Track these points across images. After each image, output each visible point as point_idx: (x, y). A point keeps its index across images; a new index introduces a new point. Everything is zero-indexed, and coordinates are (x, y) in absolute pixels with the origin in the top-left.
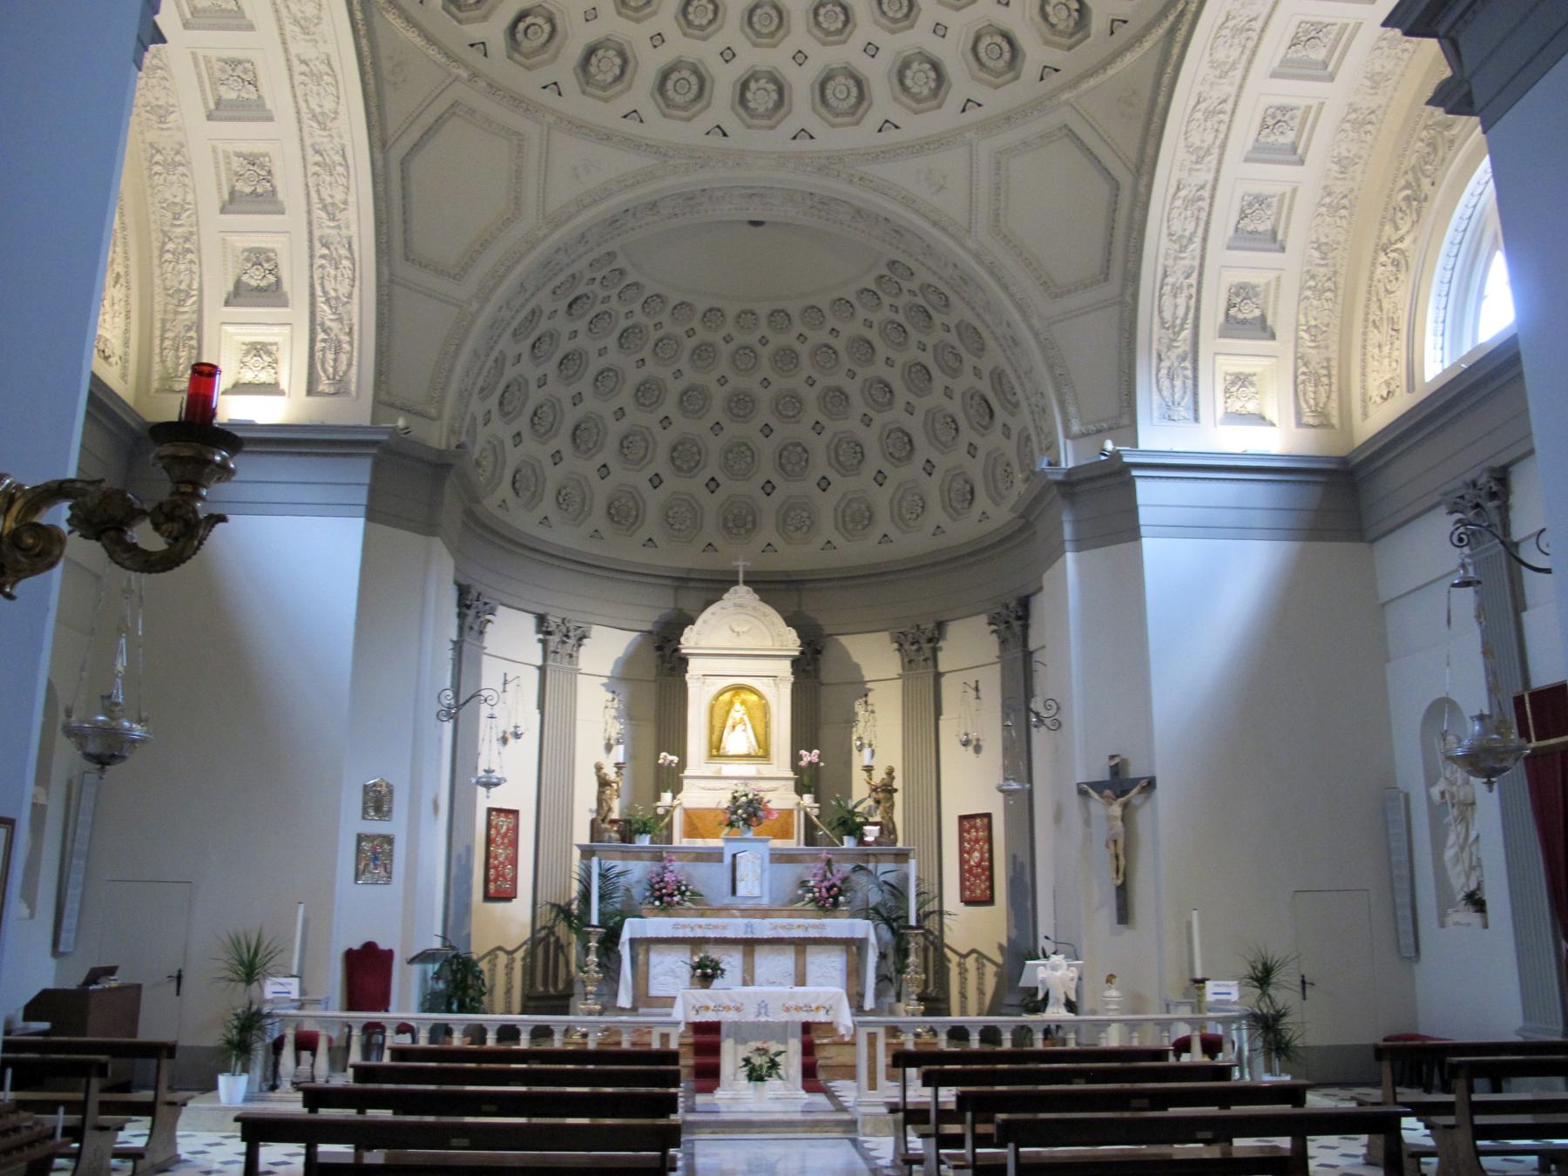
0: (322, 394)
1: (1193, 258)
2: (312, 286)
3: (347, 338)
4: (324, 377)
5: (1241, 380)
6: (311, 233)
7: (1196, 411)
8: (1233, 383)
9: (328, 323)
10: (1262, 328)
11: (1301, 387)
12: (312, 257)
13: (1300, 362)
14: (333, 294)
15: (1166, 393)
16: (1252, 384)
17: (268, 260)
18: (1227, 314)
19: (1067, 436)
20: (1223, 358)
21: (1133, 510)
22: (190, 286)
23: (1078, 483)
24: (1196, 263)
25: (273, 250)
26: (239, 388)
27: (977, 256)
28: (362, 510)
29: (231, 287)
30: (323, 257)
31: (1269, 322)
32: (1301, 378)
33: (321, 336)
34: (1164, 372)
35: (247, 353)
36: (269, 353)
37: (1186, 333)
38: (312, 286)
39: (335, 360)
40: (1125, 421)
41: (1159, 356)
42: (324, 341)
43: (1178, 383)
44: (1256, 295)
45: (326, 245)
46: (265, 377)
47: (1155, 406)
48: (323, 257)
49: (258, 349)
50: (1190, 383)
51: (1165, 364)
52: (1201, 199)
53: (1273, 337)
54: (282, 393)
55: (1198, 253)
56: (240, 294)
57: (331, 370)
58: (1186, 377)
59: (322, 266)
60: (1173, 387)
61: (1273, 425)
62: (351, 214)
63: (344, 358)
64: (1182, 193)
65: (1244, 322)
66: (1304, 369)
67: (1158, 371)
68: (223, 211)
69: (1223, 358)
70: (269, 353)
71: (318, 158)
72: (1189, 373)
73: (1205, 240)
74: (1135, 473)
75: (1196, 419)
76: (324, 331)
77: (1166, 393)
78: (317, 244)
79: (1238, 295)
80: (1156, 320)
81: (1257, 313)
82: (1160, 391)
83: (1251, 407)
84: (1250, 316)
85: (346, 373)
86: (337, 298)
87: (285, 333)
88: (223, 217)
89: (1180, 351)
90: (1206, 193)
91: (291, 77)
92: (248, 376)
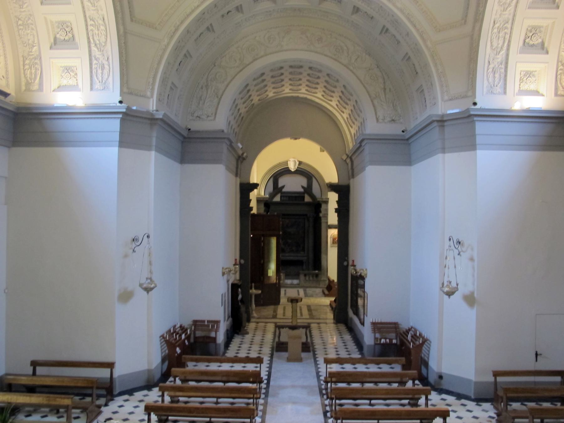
0: (97, 90)
1: (510, 14)
2: (88, 38)
3: (107, 63)
4: (98, 82)
5: (529, 74)
6: (85, 16)
7: (505, 88)
8: (525, 75)
9: (97, 56)
10: (542, 48)
11: (559, 76)
12: (87, 25)
13: (560, 64)
14: (98, 42)
15: (491, 80)
16: (534, 75)
17: (67, 27)
18: (524, 41)
19: (442, 100)
20: (520, 64)
21: (474, 135)
22: (34, 42)
23: (446, 121)
24: (511, 17)
25: (69, 22)
26: (61, 88)
27: (401, 11)
28: (118, 143)
29: (52, 40)
30: (91, 25)
31: (546, 45)
32: (559, 72)
33: (94, 62)
34: (490, 70)
35: (63, 71)
36: (73, 71)
37: (503, 52)
38: (88, 38)
39: (102, 73)
40: (470, 94)
41: (489, 62)
42: (97, 64)
43: (497, 75)
44: (540, 32)
45: (92, 20)
46: (72, 82)
47: (485, 86)
48: (91, 25)
49: (68, 69)
50: (503, 76)
51: (491, 66)
52: (506, 28)
53: (547, 53)
54: (79, 90)
55: (512, 11)
56: (56, 43)
57: (100, 78)
58: (506, 33)
59: (92, 30)
60: (494, 77)
61: (543, 95)
62: (109, 46)
63: (106, 71)
64: (497, 26)
65: (533, 46)
66: (561, 67)
67: (488, 69)
68: (51, 48)
69: (520, 64)
70: (73, 71)
71: (92, 23)
72: (503, 70)
73: (516, 6)
74: (475, 119)
75: (505, 93)
76: (96, 59)
77: (491, 80)
78: (88, 20)
79: (531, 31)
80: (489, 44)
81: (540, 40)
82: (488, 80)
83: (532, 87)
84: (536, 43)
85: (107, 79)
86: (100, 43)
87: (77, 59)
88: (52, 51)
89: (499, 60)
90: (509, 26)
91: (87, 29)
92: (64, 82)
